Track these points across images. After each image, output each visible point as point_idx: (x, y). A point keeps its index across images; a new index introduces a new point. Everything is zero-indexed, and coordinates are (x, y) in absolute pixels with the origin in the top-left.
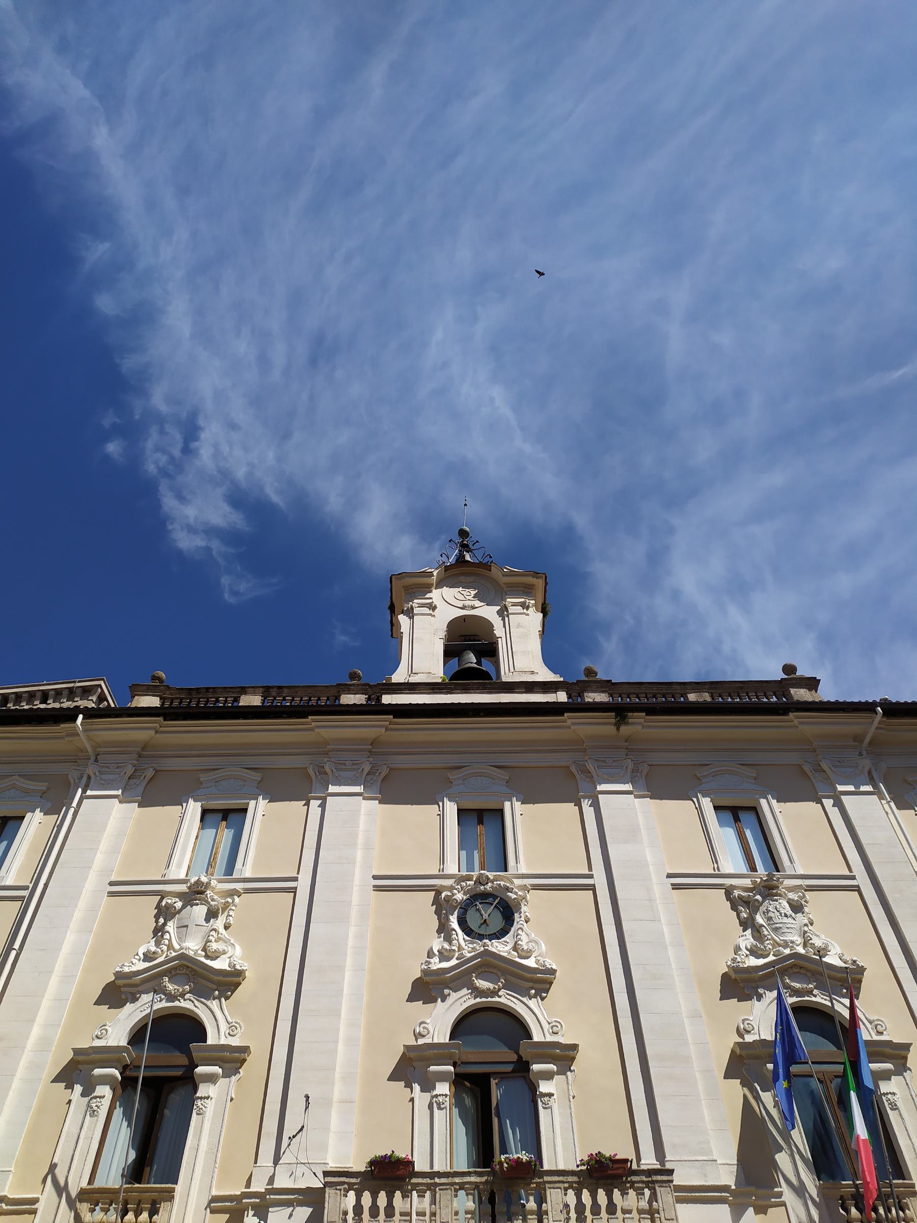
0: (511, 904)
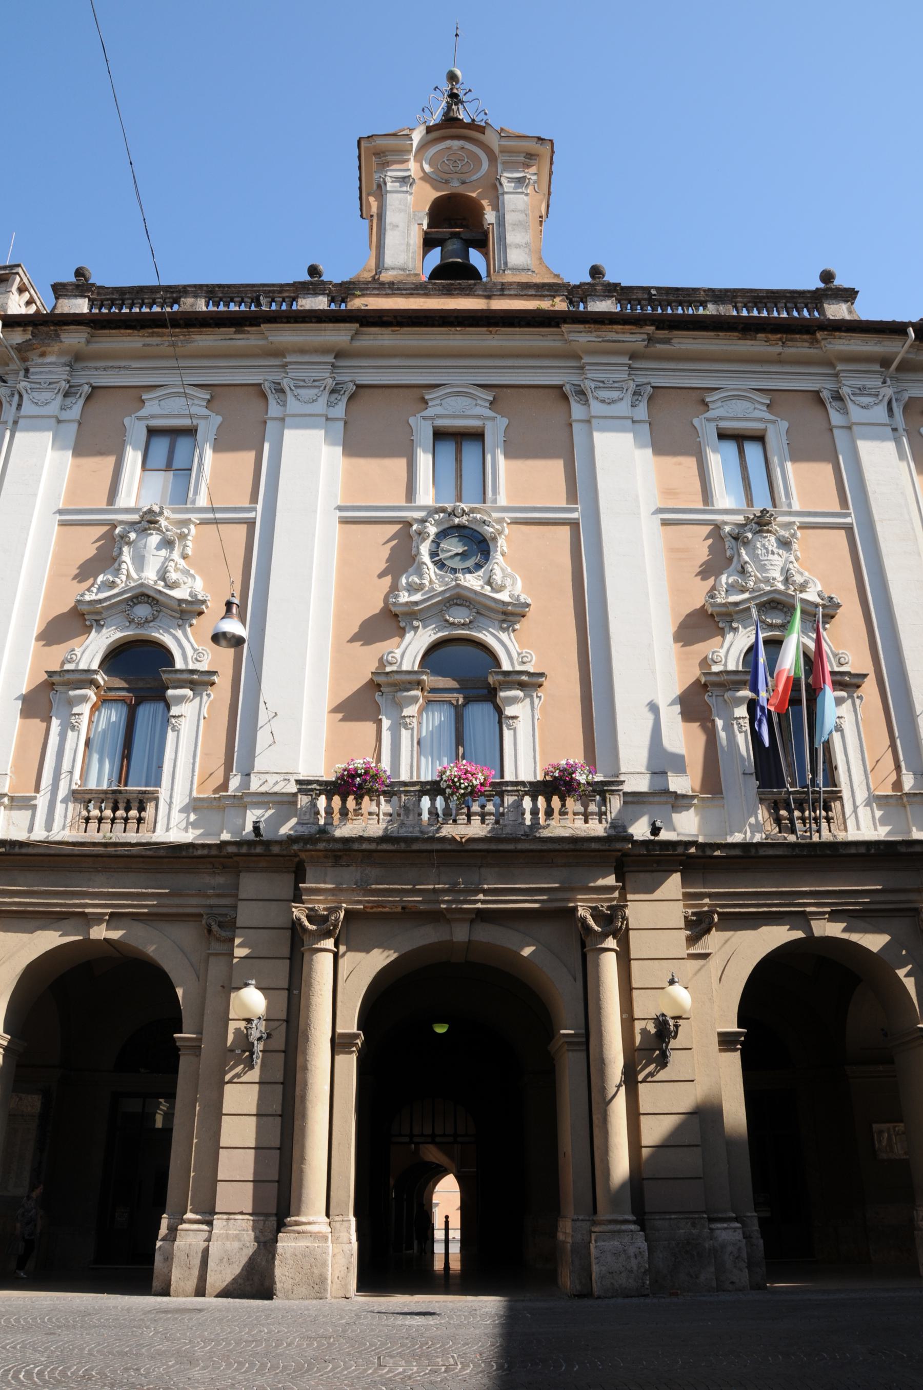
0: (488, 536)
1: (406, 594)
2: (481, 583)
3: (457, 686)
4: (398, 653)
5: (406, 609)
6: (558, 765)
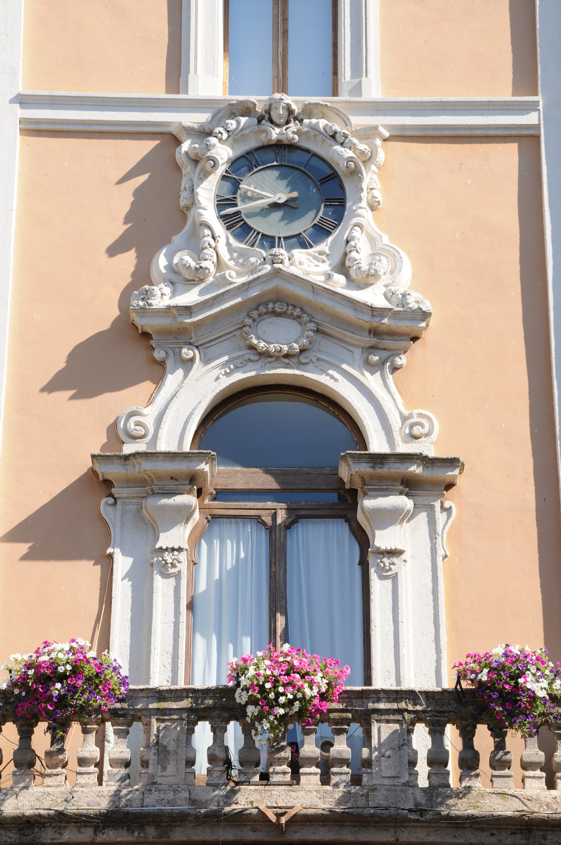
0: (341, 167)
1: (167, 290)
2: (326, 267)
3: (274, 485)
4: (149, 415)
5: (165, 322)
6: (487, 656)
